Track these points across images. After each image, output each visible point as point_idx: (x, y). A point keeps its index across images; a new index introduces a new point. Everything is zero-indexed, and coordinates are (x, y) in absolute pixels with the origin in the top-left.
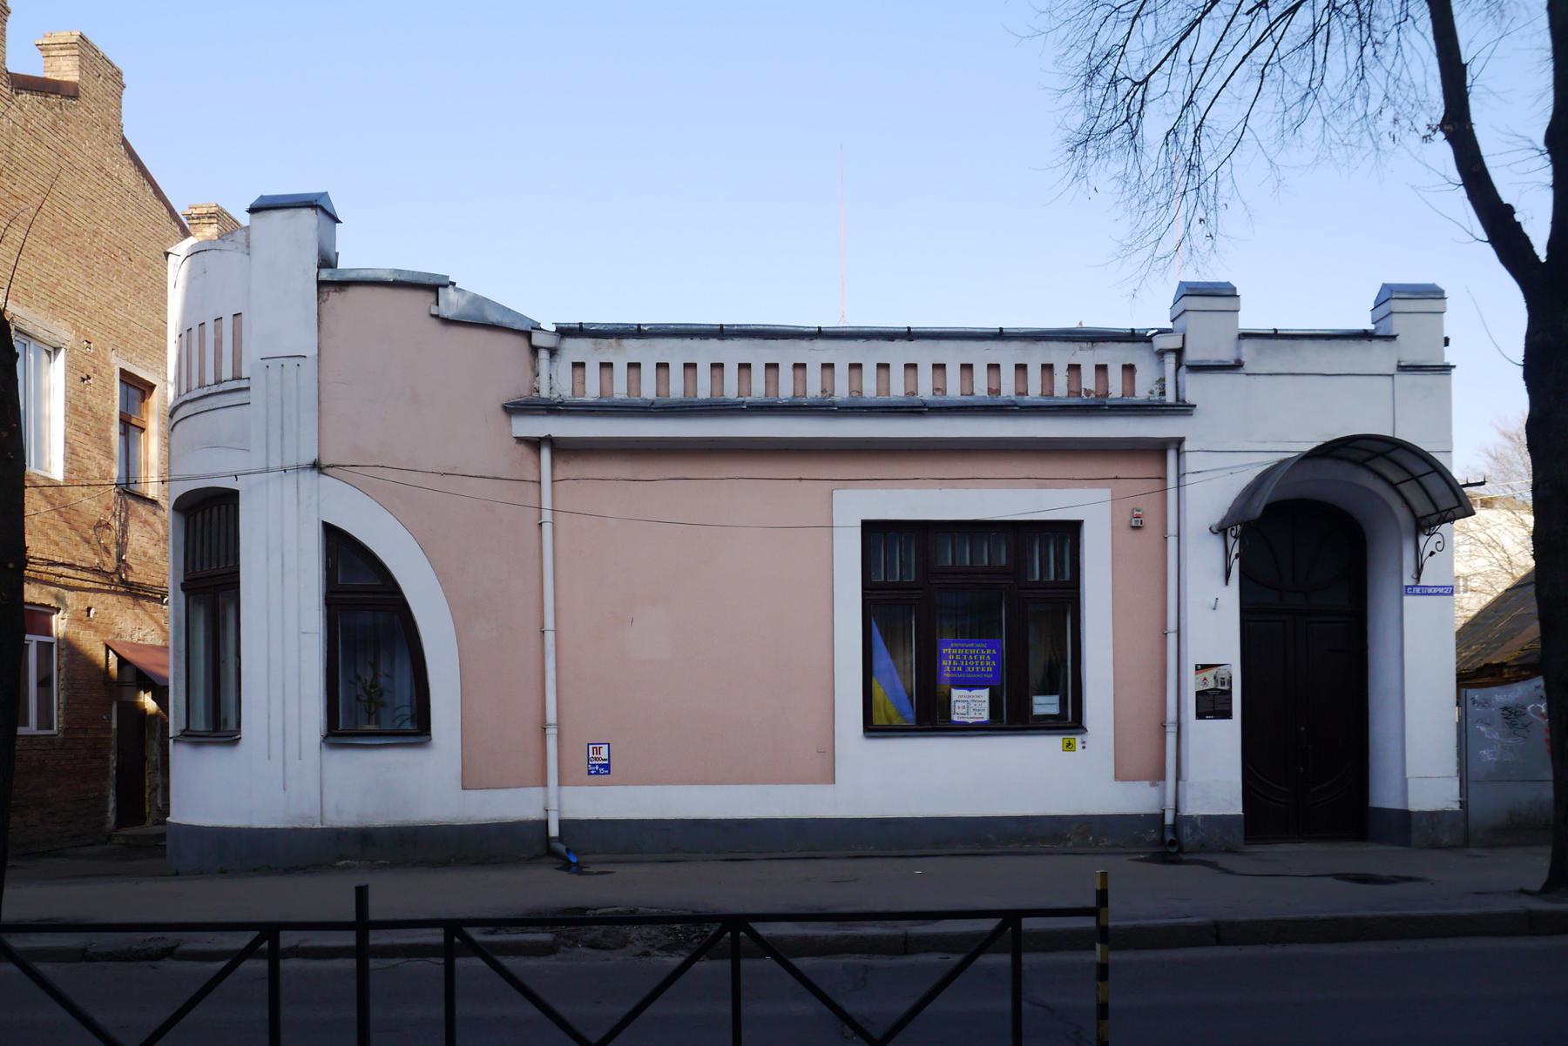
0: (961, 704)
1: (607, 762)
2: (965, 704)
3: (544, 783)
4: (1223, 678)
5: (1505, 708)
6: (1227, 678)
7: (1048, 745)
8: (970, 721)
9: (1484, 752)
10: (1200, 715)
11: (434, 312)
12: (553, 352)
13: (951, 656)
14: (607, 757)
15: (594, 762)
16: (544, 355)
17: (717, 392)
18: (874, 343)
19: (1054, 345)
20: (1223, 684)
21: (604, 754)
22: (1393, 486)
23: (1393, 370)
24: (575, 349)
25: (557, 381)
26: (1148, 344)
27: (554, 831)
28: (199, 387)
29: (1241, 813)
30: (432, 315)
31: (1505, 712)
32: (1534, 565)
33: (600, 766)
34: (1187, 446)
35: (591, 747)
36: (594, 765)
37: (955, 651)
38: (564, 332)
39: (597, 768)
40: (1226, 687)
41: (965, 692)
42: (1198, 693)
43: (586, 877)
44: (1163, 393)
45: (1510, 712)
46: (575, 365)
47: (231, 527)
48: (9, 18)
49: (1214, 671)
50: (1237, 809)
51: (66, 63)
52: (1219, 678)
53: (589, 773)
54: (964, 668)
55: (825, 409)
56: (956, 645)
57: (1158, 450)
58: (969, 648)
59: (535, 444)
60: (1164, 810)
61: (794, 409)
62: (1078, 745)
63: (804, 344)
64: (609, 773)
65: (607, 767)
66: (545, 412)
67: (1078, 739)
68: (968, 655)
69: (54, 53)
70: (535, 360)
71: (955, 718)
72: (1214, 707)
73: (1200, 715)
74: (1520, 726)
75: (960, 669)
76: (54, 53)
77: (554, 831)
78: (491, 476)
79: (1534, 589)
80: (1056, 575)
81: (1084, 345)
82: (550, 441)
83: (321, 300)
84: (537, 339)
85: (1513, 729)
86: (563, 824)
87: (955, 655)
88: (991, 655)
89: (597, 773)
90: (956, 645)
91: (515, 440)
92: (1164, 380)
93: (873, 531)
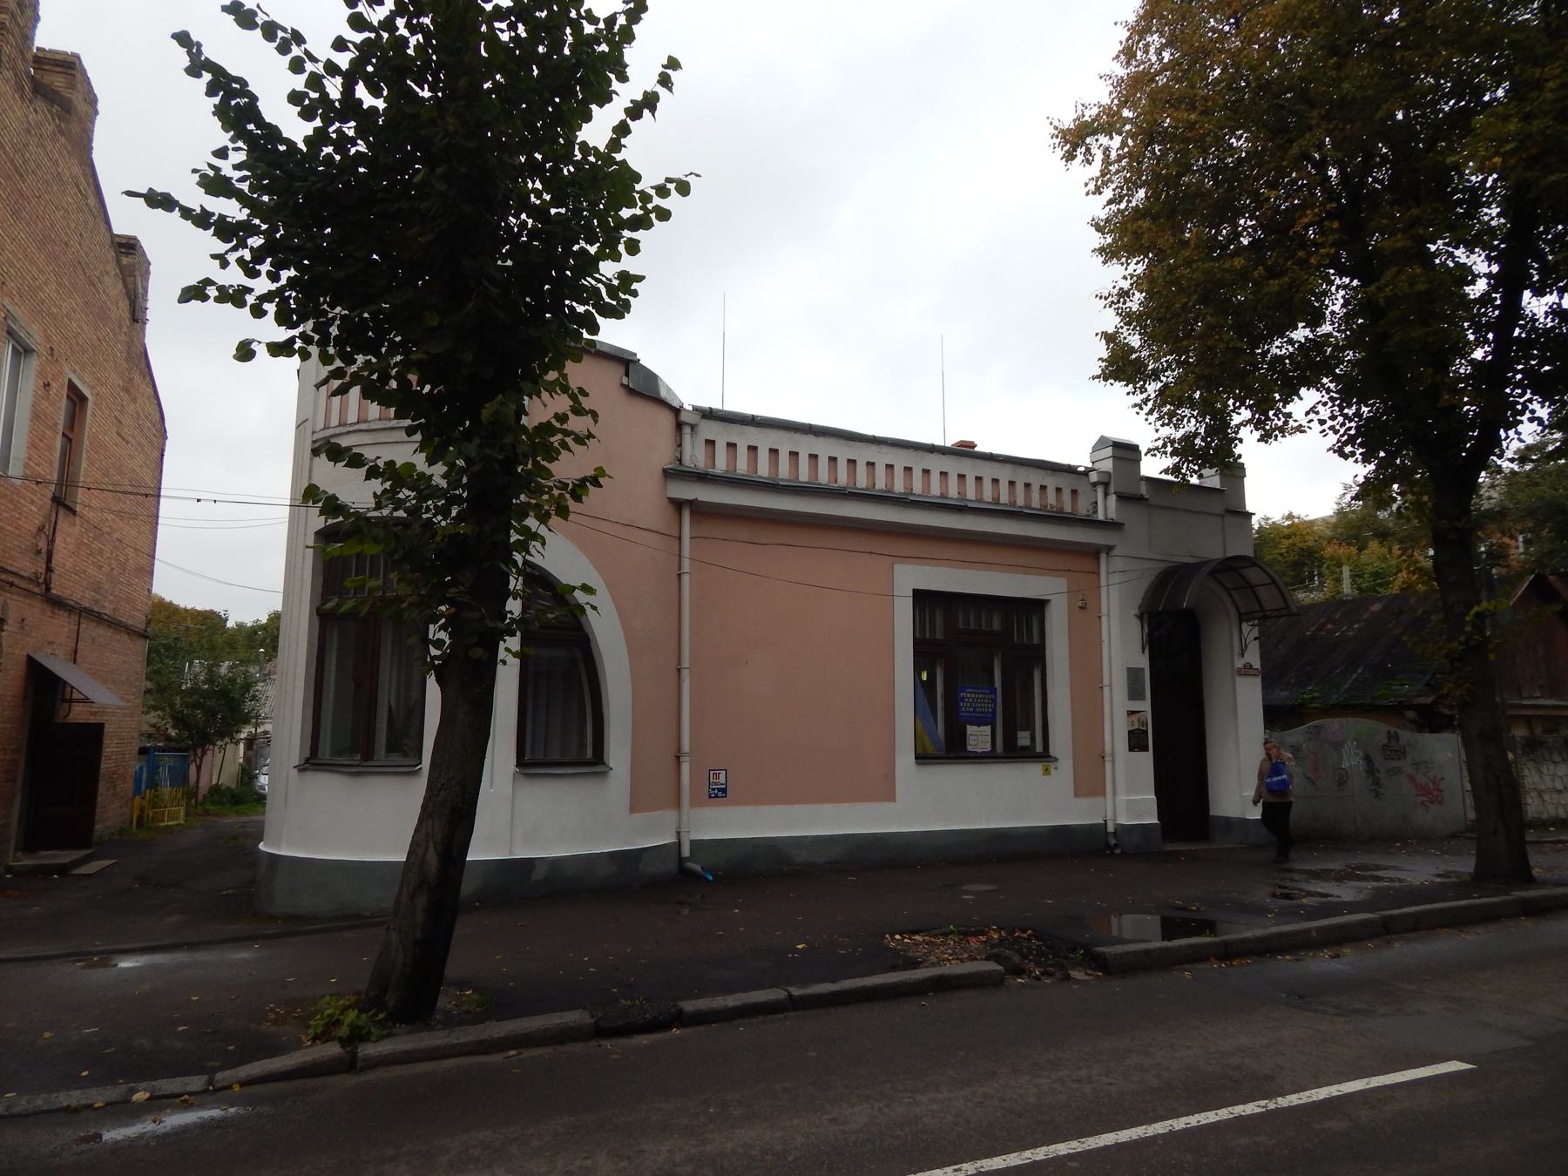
0: (973, 738)
1: (724, 786)
2: (975, 737)
3: (678, 804)
6: (1145, 720)
7: (1034, 770)
8: (979, 751)
11: (625, 380)
12: (693, 427)
13: (970, 699)
14: (724, 782)
15: (714, 787)
16: (687, 430)
17: (731, 468)
18: (920, 453)
19: (1032, 470)
21: (722, 780)
22: (1227, 590)
23: (1222, 513)
24: (709, 430)
25: (695, 456)
26: (795, 458)
27: (686, 852)
28: (380, 419)
29: (1156, 821)
30: (622, 385)
33: (719, 790)
34: (1116, 552)
35: (712, 772)
36: (713, 789)
37: (969, 695)
38: (709, 414)
39: (716, 791)
40: (1144, 728)
41: (975, 728)
44: (1096, 512)
46: (707, 441)
49: (1137, 715)
50: (1153, 820)
51: (60, 79)
53: (710, 797)
54: (974, 708)
55: (772, 487)
56: (970, 690)
57: (1094, 553)
58: (979, 693)
59: (678, 505)
60: (1105, 821)
61: (772, 487)
62: (1053, 771)
63: (874, 447)
64: (726, 796)
65: (724, 791)
66: (695, 479)
67: (1052, 765)
68: (977, 699)
69: (47, 67)
75: (972, 709)
76: (47, 67)
77: (686, 852)
80: (931, 635)
81: (1049, 472)
82: (693, 504)
84: (683, 417)
86: (695, 844)
87: (969, 698)
88: (964, 702)
89: (716, 796)
90: (970, 690)
91: (665, 503)
92: (1096, 503)
93: (924, 600)
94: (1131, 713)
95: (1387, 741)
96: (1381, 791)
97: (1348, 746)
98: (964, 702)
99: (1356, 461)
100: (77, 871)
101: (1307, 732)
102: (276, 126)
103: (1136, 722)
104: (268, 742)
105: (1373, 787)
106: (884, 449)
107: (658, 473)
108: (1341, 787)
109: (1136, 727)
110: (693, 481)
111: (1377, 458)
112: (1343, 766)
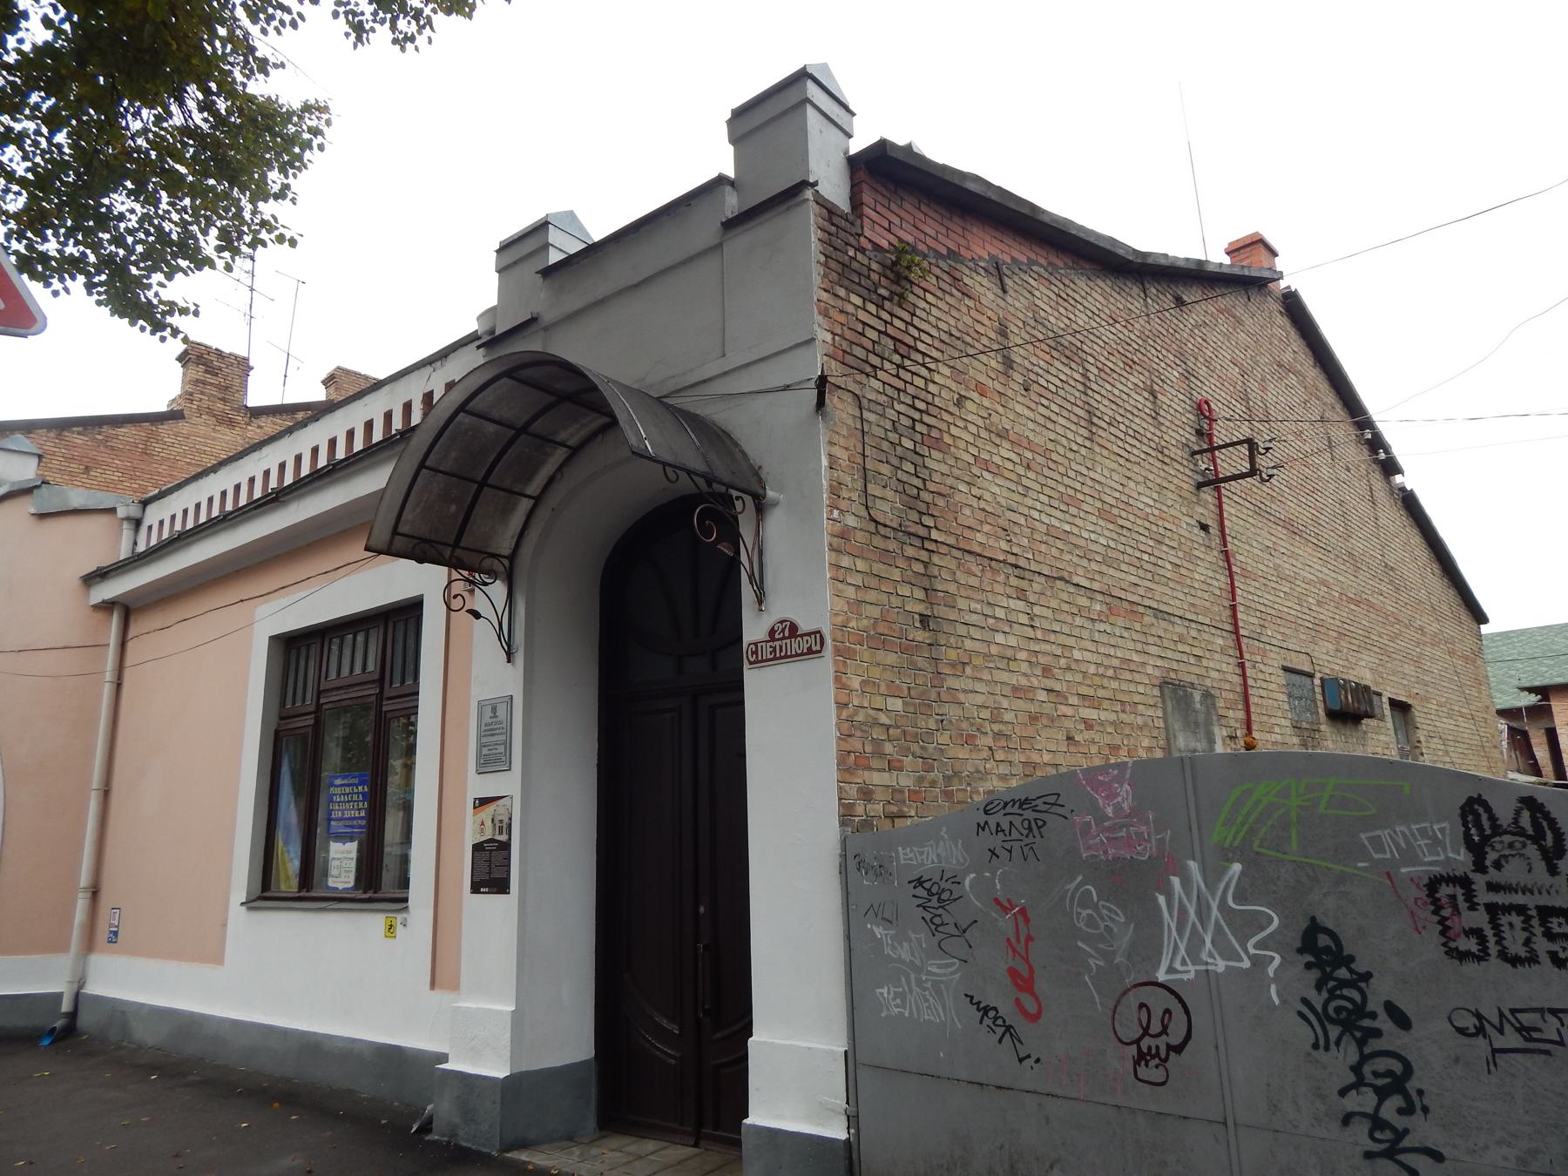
4: (501, 821)
5: (919, 882)
9: (885, 991)
10: (476, 888)
20: (501, 833)
31: (920, 892)
32: (1400, 1097)
40: (504, 838)
42: (477, 848)
43: (80, 1007)
45: (929, 891)
47: (411, 642)
48: (251, 373)
49: (491, 808)
52: (496, 821)
59: (107, 606)
66: (98, 579)
70: (1406, 723)
71: (331, 883)
72: (490, 873)
73: (476, 888)
74: (952, 930)
78: (62, 645)
79: (354, 855)
83: (48, 442)
85: (939, 936)
94: (483, 802)
95: (1462, 859)
96: (1422, 1131)
97: (1186, 883)
98: (363, 794)
99: (328, 123)
100: (1403, 845)
101: (981, 827)
102: (908, 149)
103: (488, 823)
104: (1197, 724)
105: (1365, 1100)
106: (266, 450)
107: (77, 583)
108: (1151, 1072)
109: (488, 836)
110: (98, 583)
111: (80, 168)
112: (1161, 976)
